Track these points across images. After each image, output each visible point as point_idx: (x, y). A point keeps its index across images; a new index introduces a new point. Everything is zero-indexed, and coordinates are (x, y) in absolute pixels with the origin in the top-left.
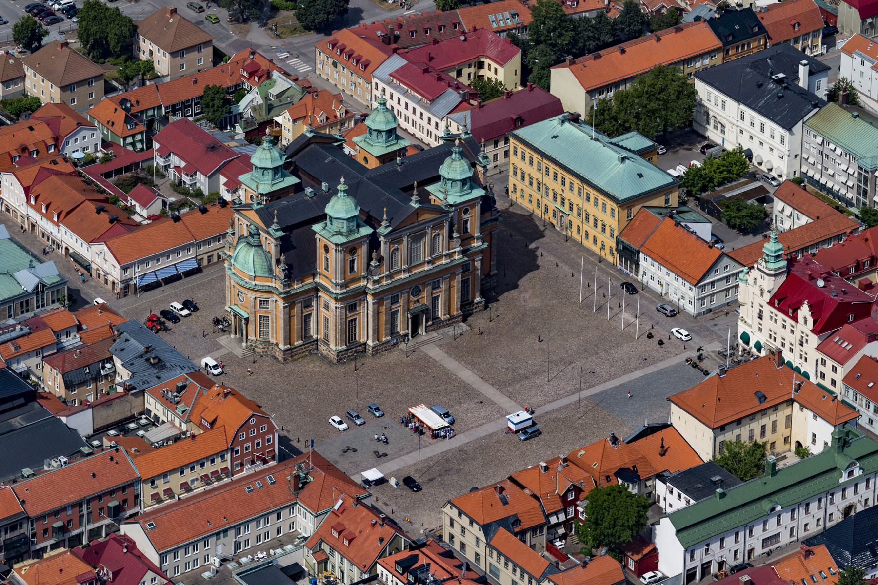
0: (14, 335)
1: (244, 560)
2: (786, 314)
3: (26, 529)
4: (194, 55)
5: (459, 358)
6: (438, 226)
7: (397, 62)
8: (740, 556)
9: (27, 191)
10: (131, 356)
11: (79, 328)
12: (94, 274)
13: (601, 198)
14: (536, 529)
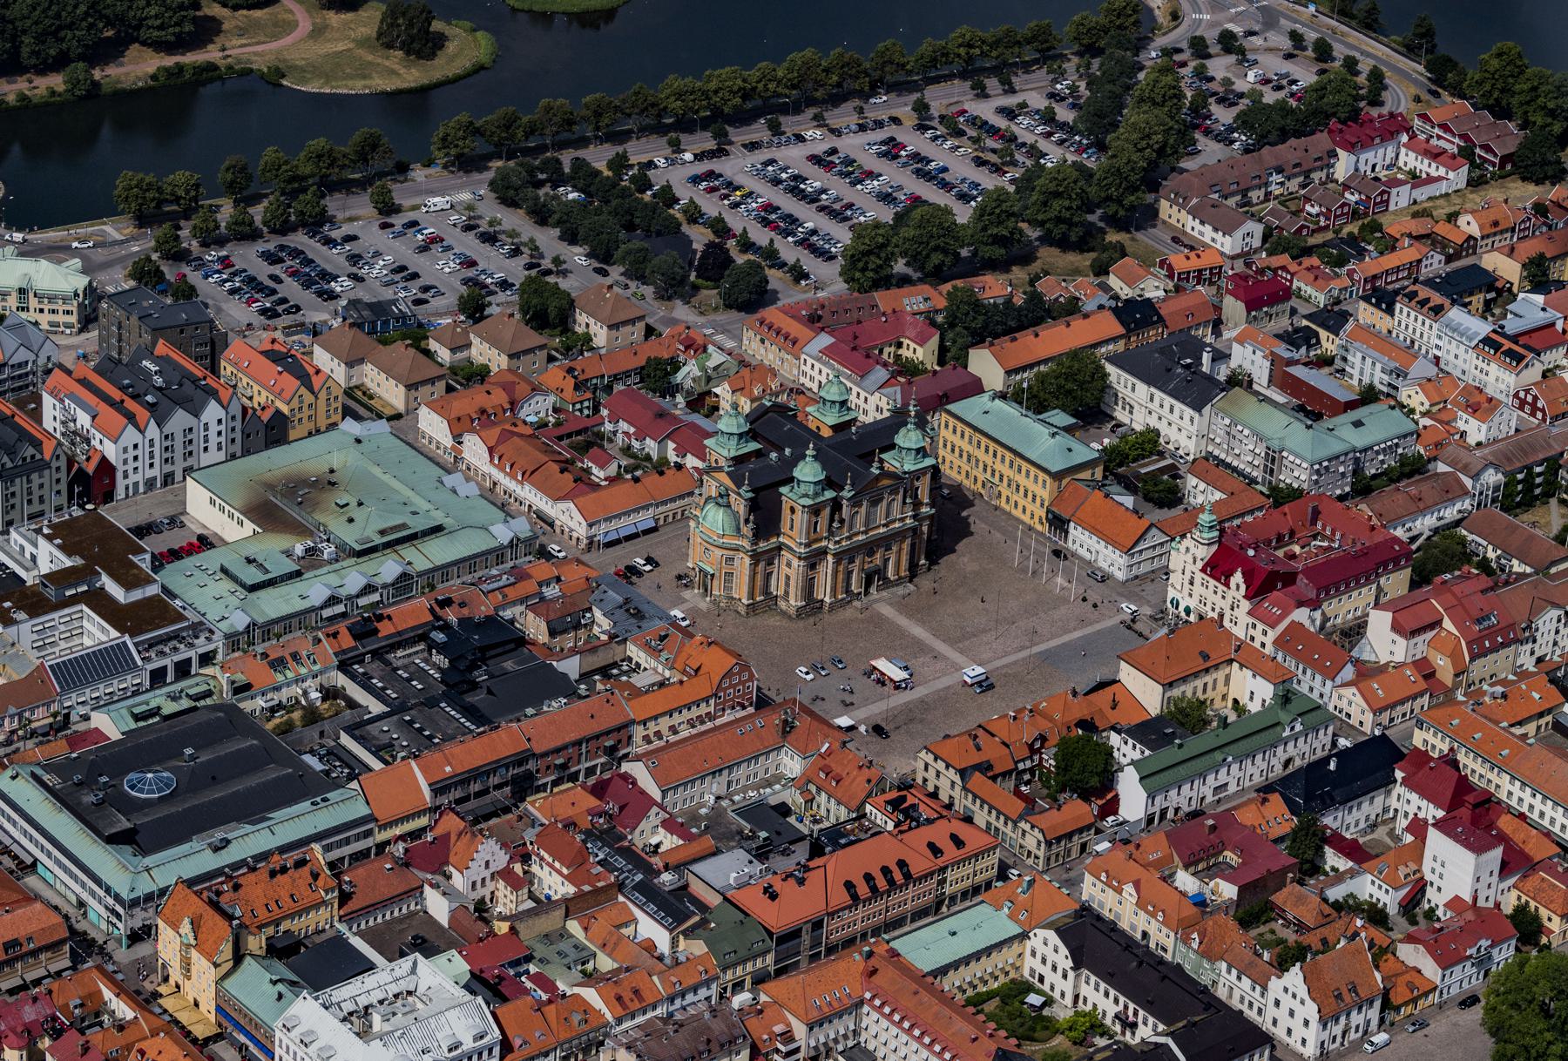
0: (501, 584)
1: (736, 798)
2: (1218, 580)
3: (531, 765)
4: (629, 328)
5: (910, 616)
6: (894, 491)
7: (825, 340)
8: (1193, 802)
9: (491, 450)
10: (610, 607)
11: (558, 579)
12: (558, 531)
13: (1033, 470)
14: (1006, 775)
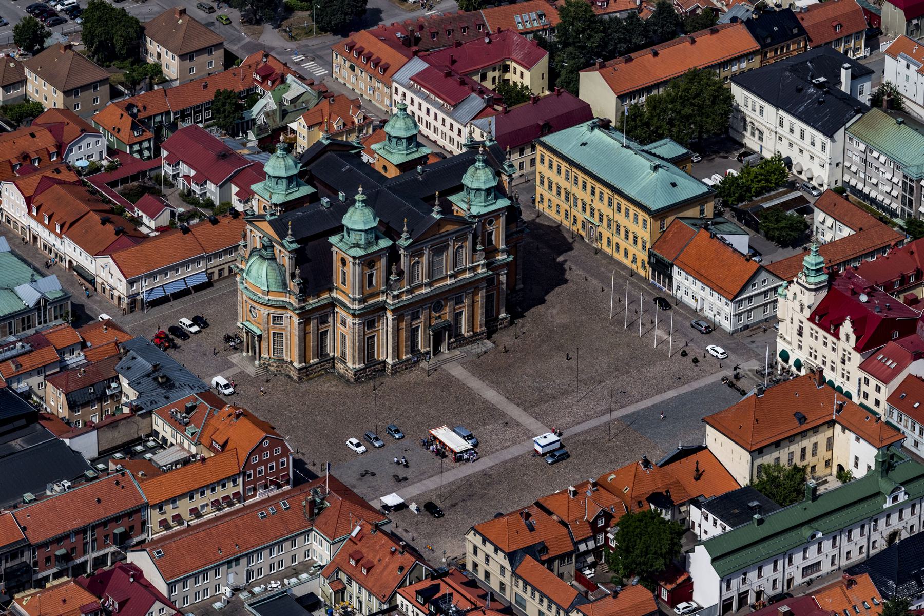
0: (14, 352)
1: (256, 590)
2: (828, 331)
3: (27, 557)
4: (205, 58)
5: (483, 377)
6: (461, 238)
7: (418, 66)
8: (779, 585)
9: (29, 201)
11: (83, 346)
12: (99, 289)
13: (633, 209)
14: (564, 557)
